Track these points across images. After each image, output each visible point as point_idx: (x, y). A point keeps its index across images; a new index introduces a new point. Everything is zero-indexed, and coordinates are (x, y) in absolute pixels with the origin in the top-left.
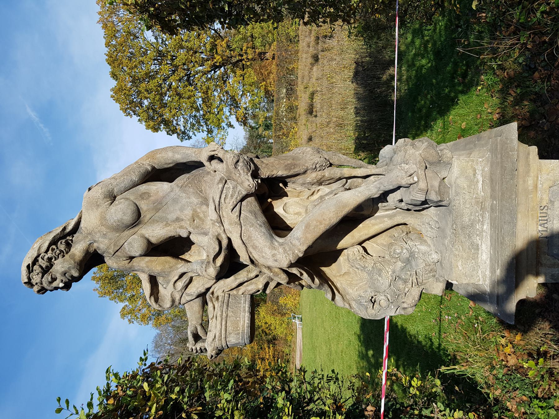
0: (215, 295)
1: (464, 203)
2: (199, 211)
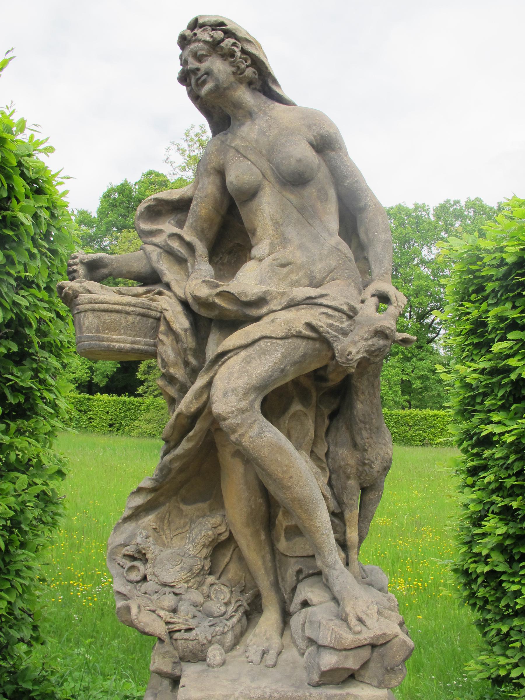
2: (301, 274)
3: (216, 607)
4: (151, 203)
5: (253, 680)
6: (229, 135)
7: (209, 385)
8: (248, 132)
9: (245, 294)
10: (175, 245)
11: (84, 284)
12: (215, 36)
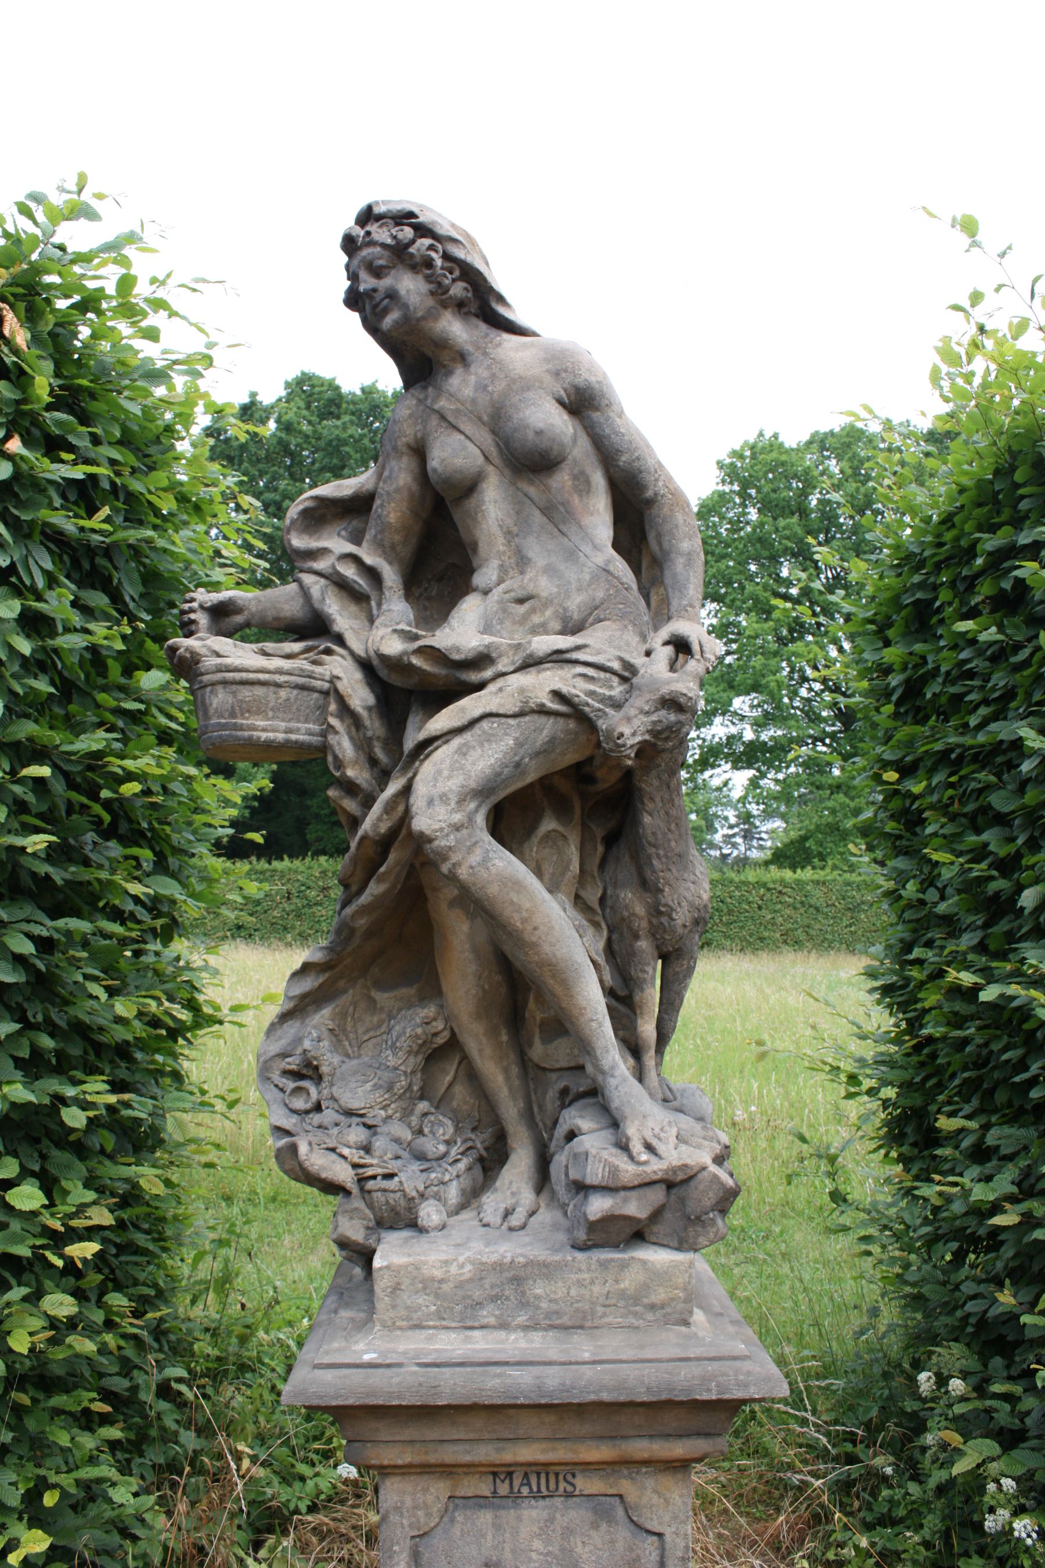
0: (326, 658)
1: (580, 1283)
2: (548, 613)
3: (434, 1146)
4: (308, 504)
5: (488, 1244)
6: (430, 389)
7: (407, 790)
8: (461, 385)
9: (458, 650)
10: (349, 571)
11: (209, 642)
12: (400, 236)
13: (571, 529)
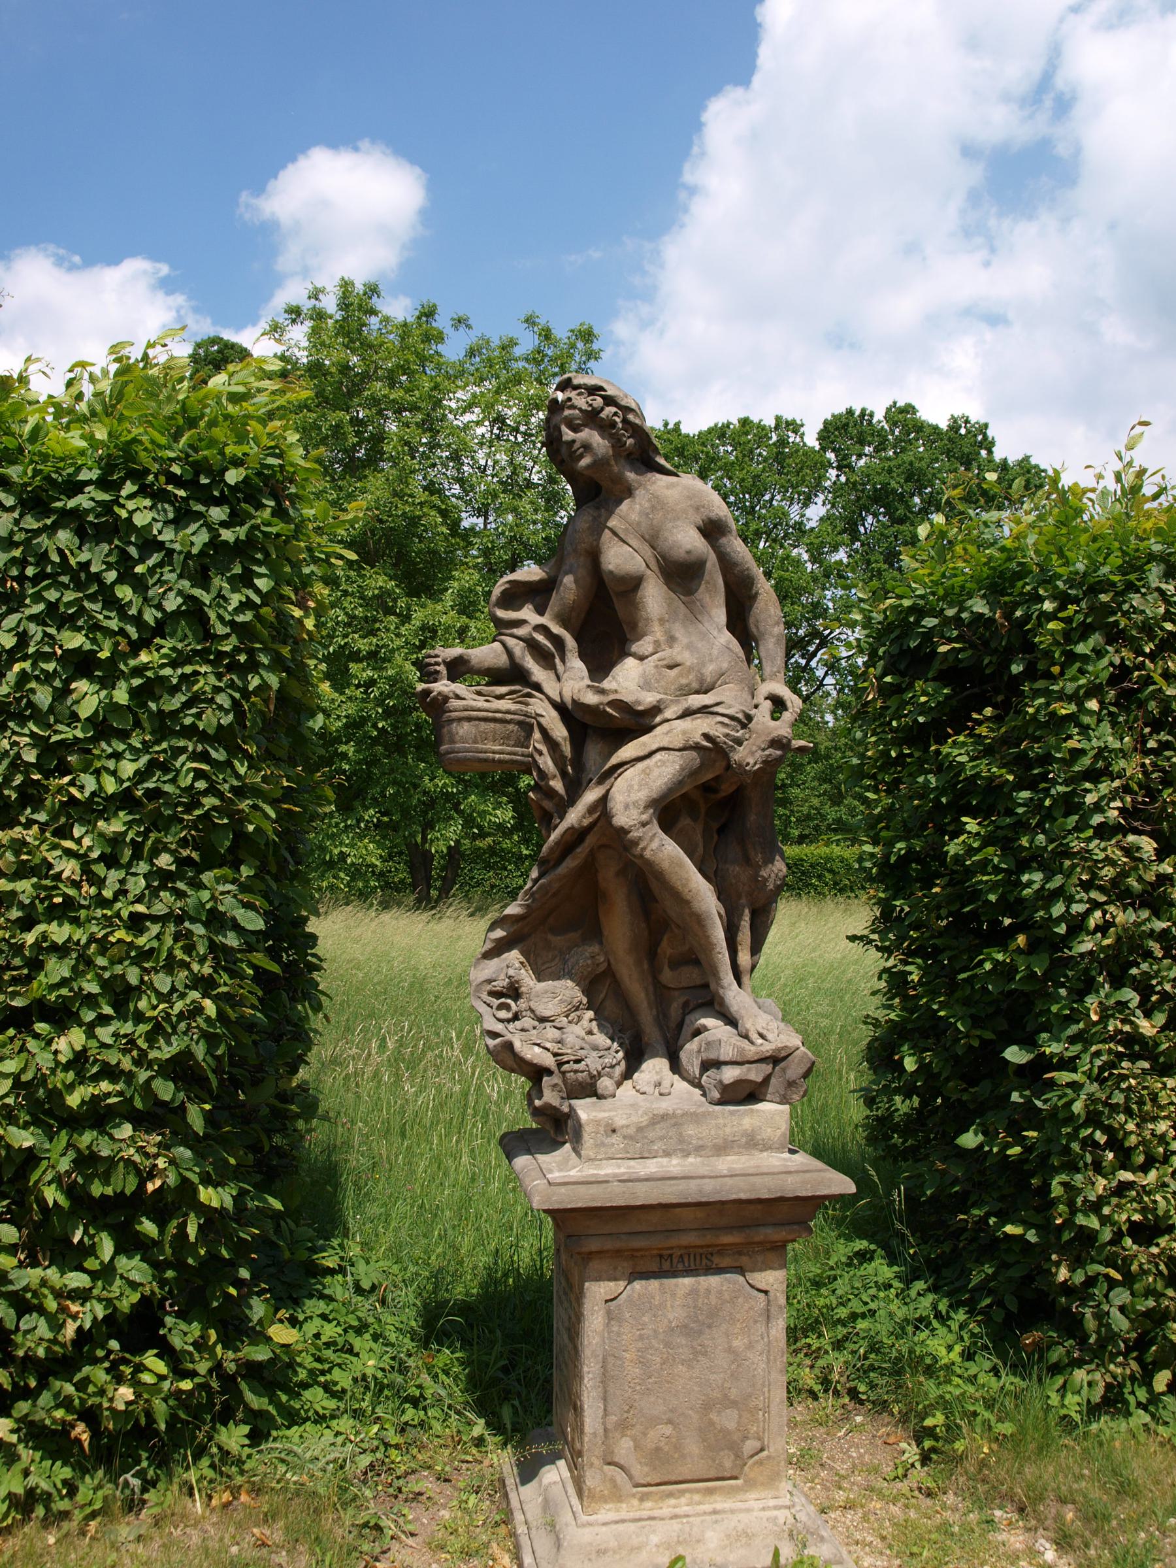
10: (540, 638)
13: (705, 619)
